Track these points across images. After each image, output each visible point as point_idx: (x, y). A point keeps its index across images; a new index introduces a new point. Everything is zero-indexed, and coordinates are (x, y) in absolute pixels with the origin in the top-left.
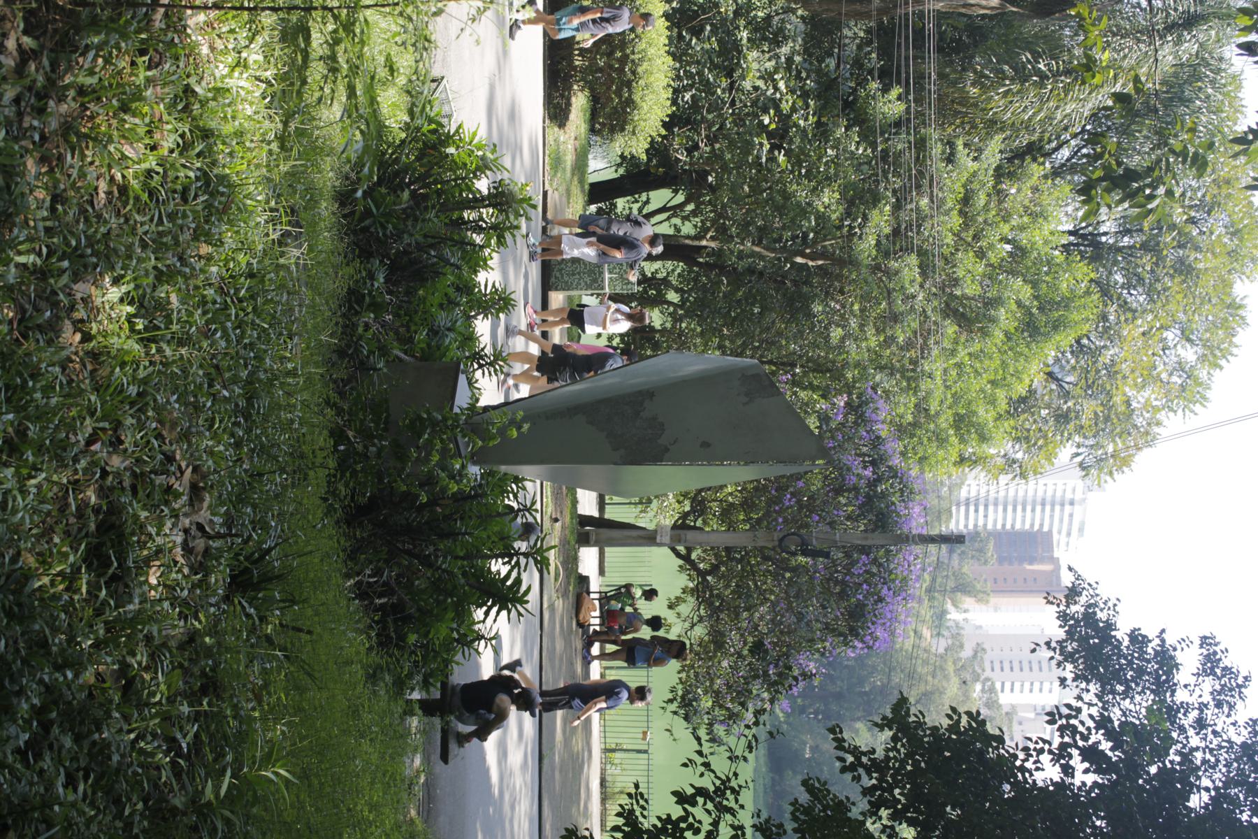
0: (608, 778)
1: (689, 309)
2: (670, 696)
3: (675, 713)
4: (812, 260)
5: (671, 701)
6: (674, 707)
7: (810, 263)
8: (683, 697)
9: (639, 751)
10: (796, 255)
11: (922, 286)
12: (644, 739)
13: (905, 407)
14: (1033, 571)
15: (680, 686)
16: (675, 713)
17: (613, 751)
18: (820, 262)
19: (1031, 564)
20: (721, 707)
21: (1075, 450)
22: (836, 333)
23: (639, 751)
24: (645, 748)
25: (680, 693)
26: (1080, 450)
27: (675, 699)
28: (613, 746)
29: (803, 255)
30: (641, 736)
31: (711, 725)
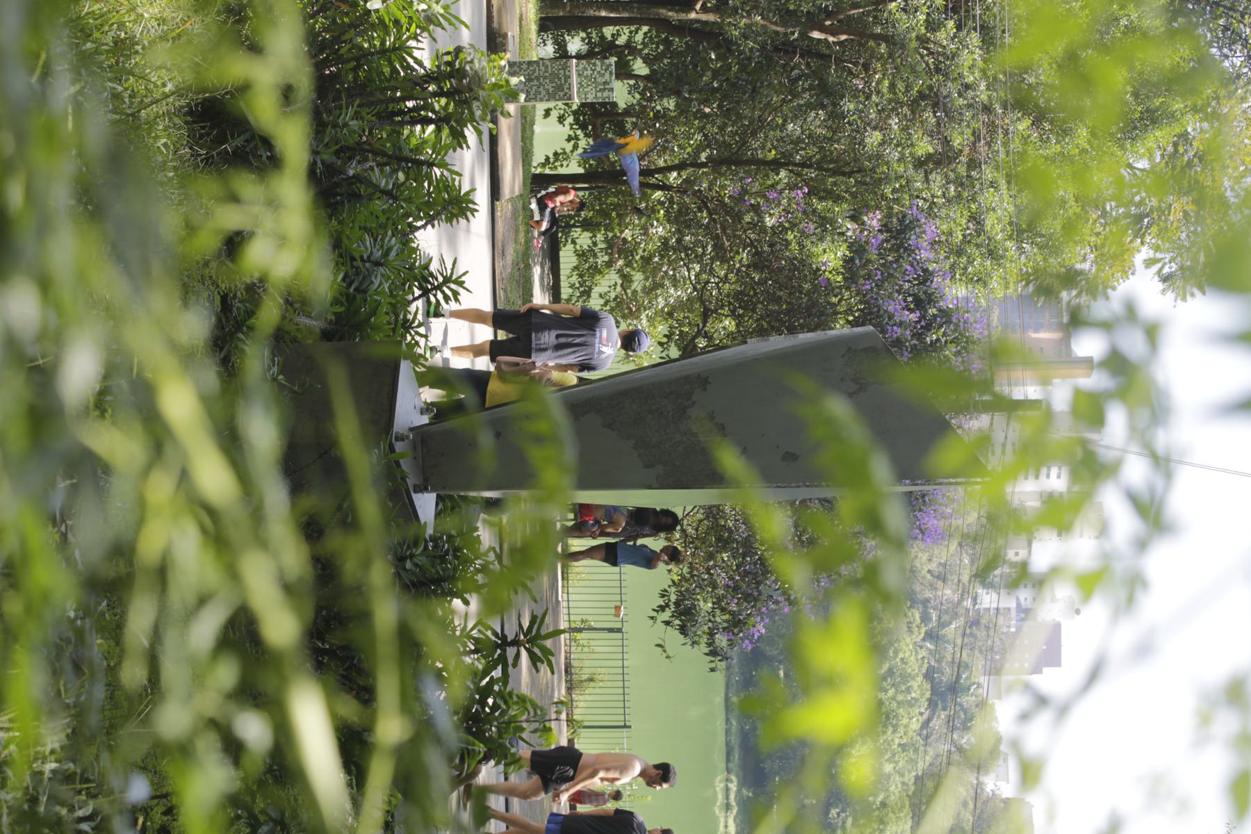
0: (574, 663)
1: (655, 83)
2: (661, 602)
3: (667, 623)
4: (833, 35)
5: (662, 608)
6: (666, 615)
7: (831, 39)
8: (677, 604)
9: (611, 630)
10: (812, 29)
11: (984, 71)
12: (617, 615)
13: (955, 222)
14: (1039, 340)
15: (673, 589)
16: (667, 623)
17: (579, 630)
18: (843, 37)
19: (1036, 331)
20: (723, 610)
21: (1151, 254)
22: (873, 138)
23: (611, 630)
24: (619, 625)
25: (673, 598)
26: (1159, 255)
27: (667, 605)
28: (578, 625)
29: (822, 29)
30: (613, 611)
31: (711, 634)
